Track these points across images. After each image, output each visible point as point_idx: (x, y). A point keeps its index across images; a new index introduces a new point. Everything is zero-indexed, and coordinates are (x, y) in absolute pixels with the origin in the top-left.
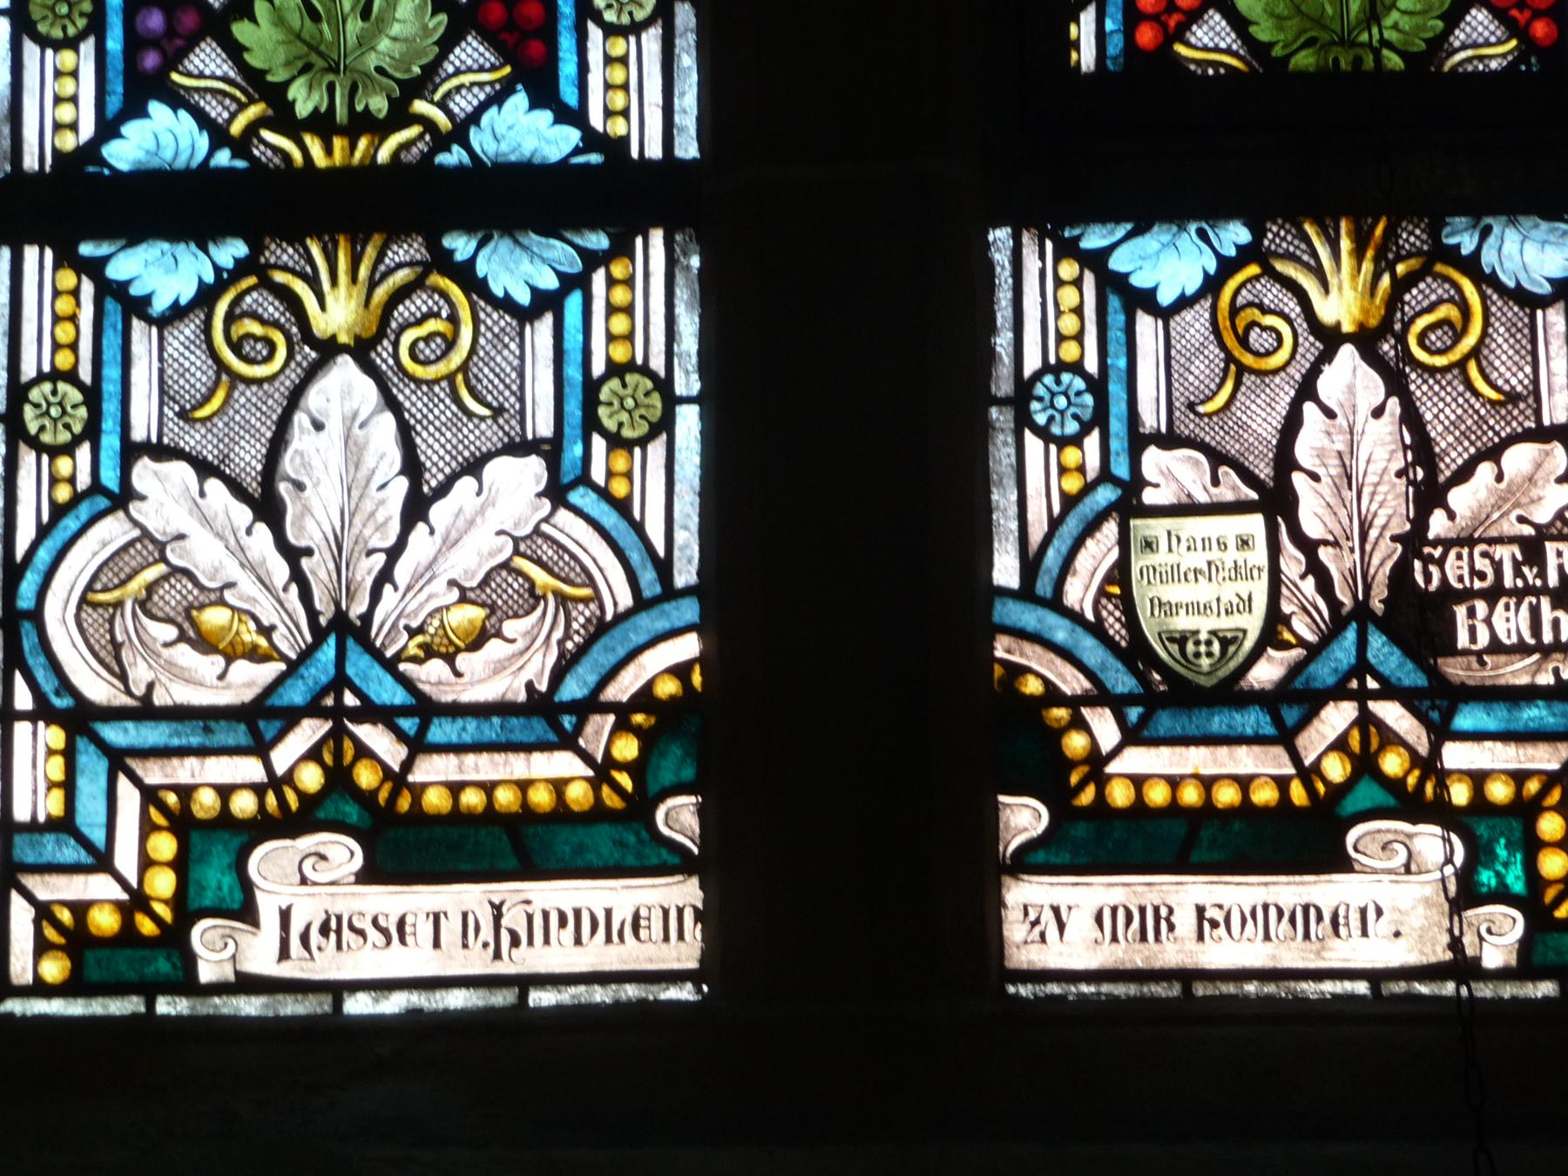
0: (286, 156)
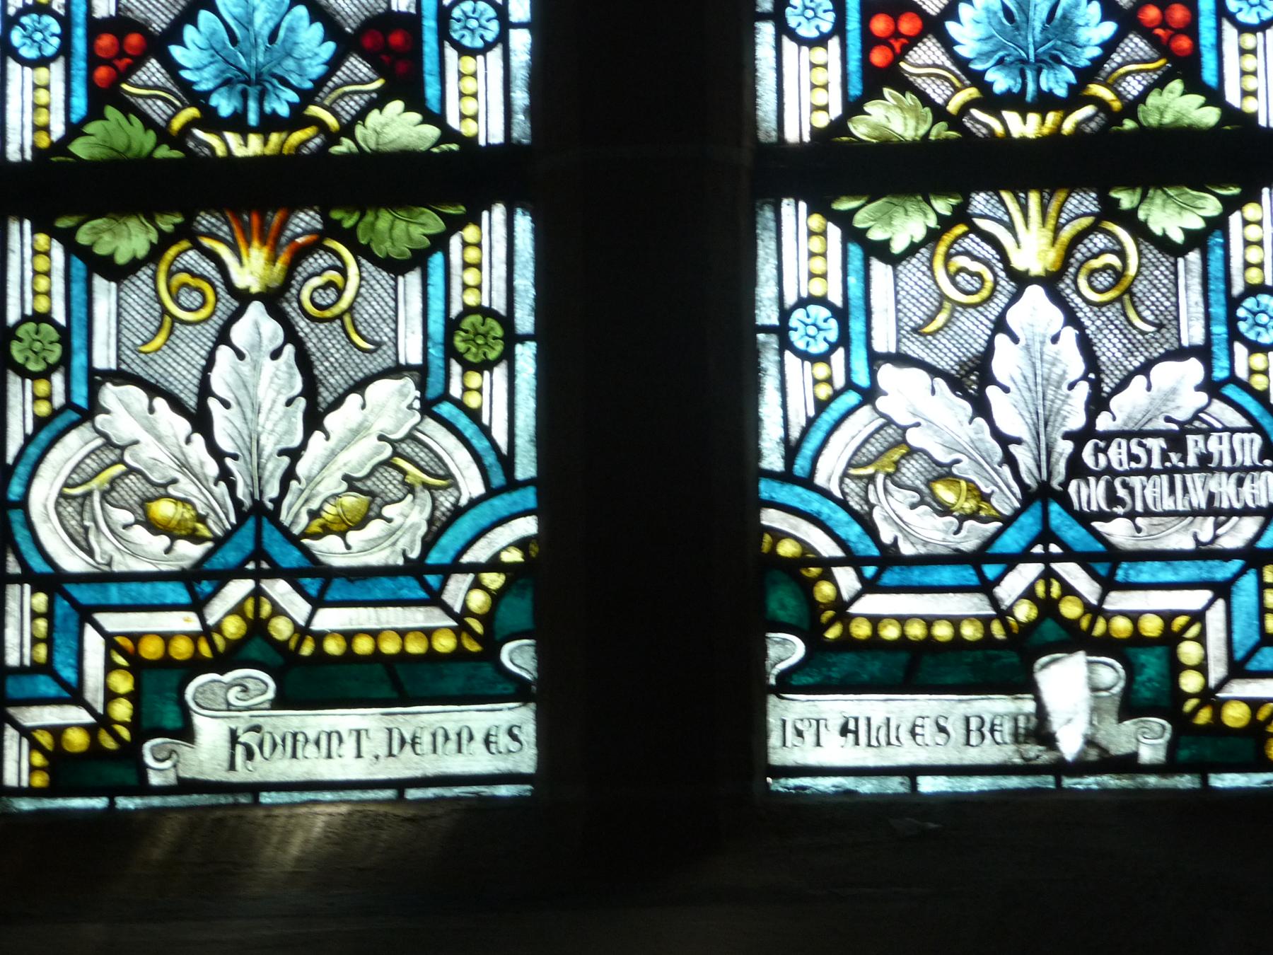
0: (991, 130)
